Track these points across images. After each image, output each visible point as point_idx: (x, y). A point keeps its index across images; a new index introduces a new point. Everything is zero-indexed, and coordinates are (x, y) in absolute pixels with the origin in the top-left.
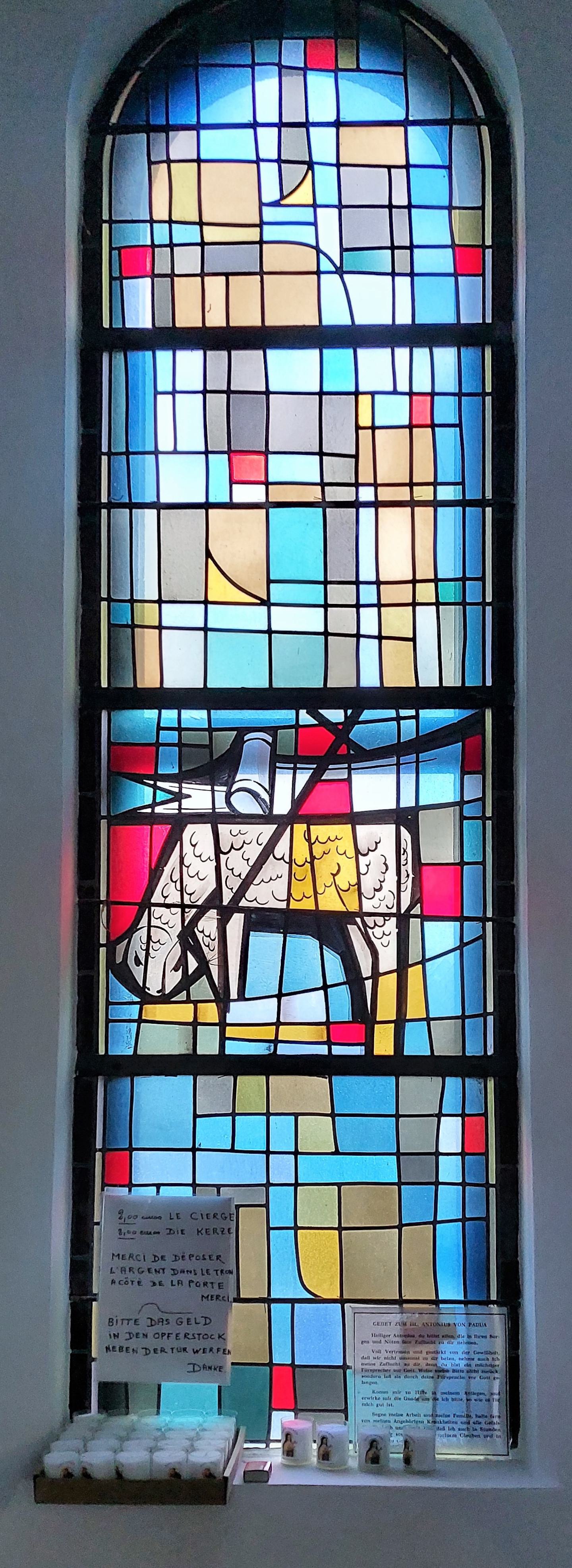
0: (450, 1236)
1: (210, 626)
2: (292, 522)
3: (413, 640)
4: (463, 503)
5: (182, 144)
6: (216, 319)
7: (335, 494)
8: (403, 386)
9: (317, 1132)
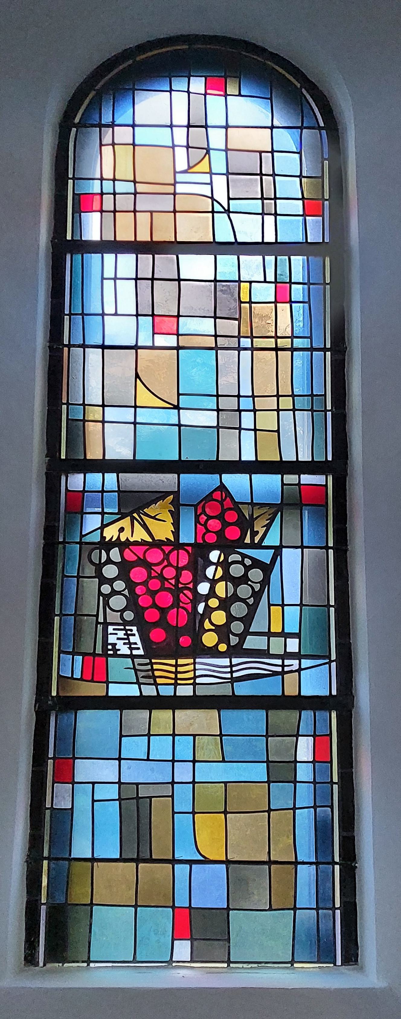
5: (123, 134)
6: (143, 236)
8: (271, 277)
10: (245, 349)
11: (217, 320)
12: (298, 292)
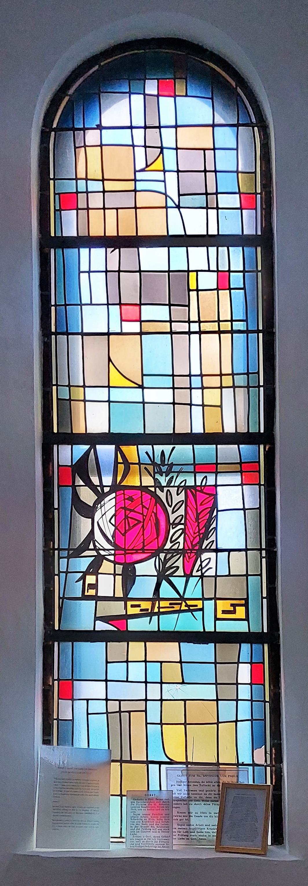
0: (245, 728)
2: (154, 367)
4: (247, 332)
5: (92, 137)
6: (111, 232)
7: (177, 327)
8: (213, 267)
10: (193, 290)
11: (172, 307)
12: (236, 280)
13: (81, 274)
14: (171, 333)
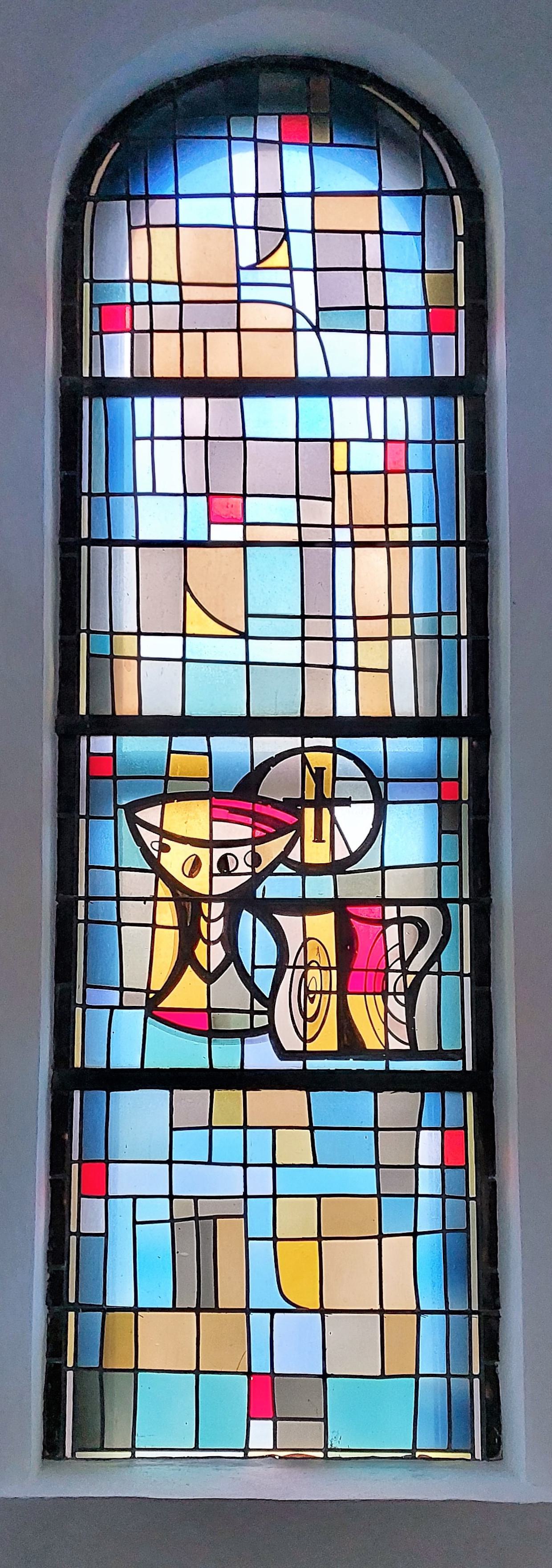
1: (188, 656)
3: (389, 671)
4: (438, 544)
5: (162, 211)
6: (193, 370)
8: (378, 434)
9: (295, 1146)
13: (137, 442)
14: (300, 544)
